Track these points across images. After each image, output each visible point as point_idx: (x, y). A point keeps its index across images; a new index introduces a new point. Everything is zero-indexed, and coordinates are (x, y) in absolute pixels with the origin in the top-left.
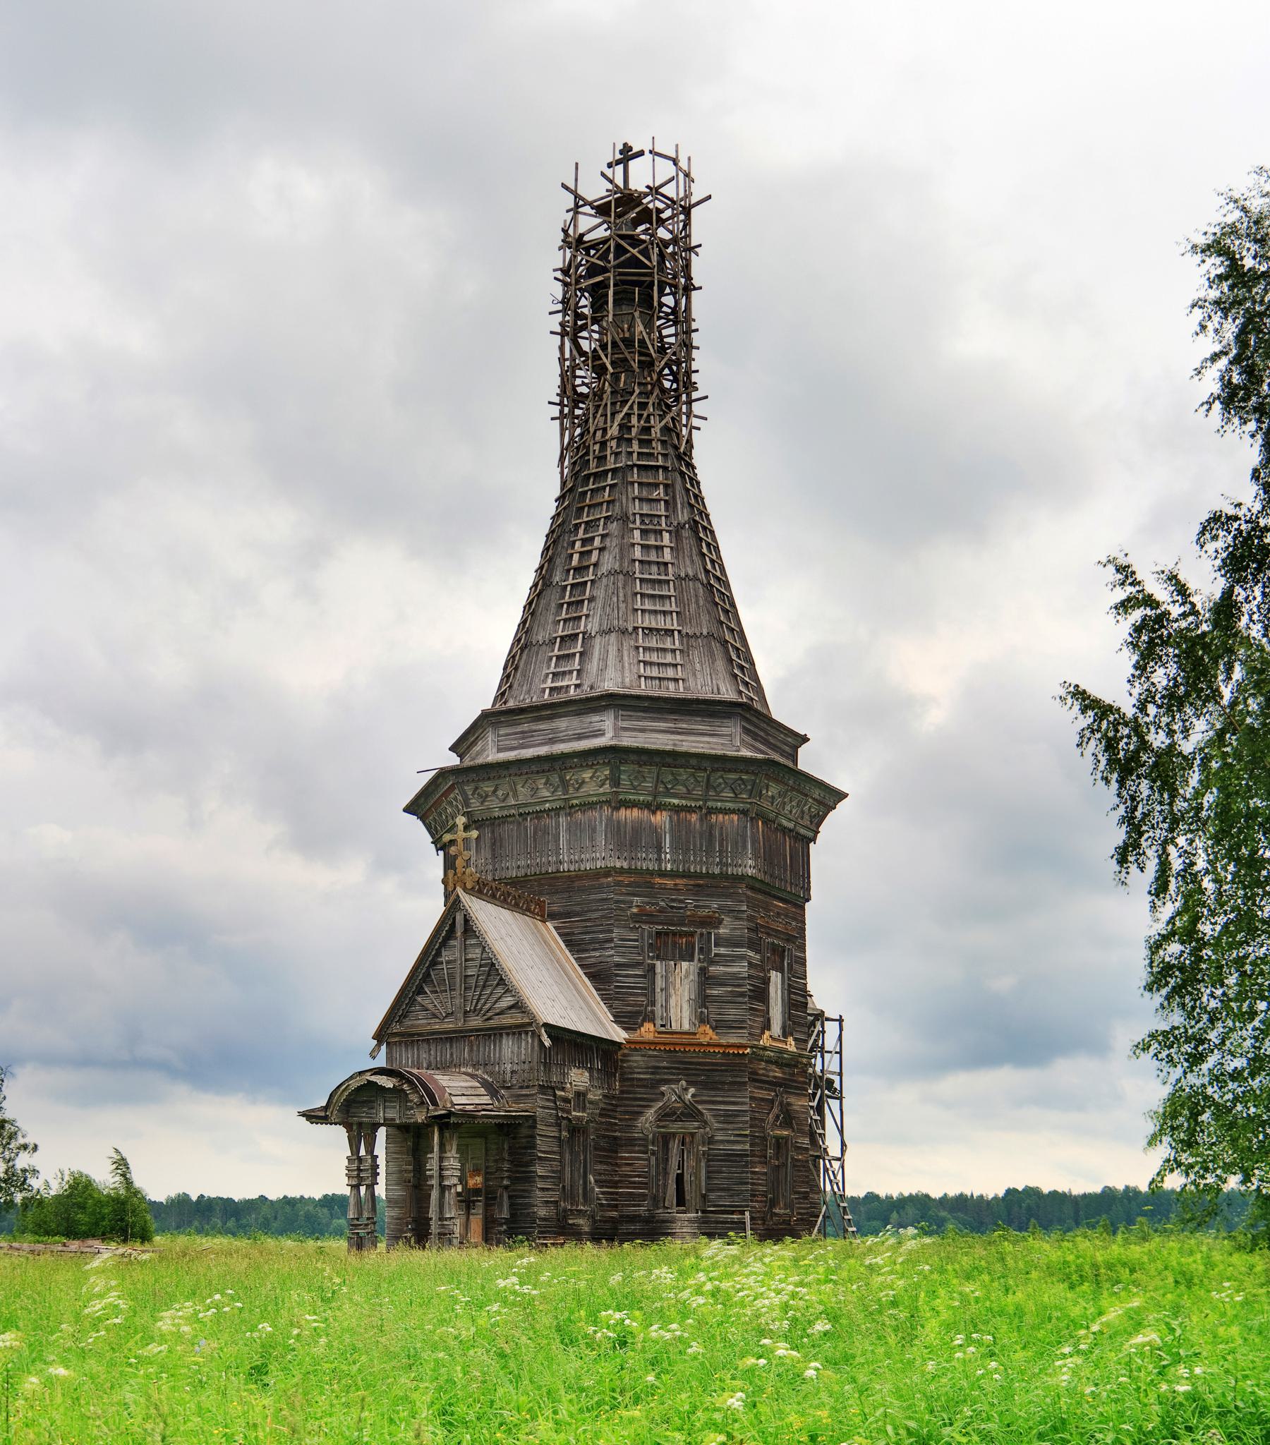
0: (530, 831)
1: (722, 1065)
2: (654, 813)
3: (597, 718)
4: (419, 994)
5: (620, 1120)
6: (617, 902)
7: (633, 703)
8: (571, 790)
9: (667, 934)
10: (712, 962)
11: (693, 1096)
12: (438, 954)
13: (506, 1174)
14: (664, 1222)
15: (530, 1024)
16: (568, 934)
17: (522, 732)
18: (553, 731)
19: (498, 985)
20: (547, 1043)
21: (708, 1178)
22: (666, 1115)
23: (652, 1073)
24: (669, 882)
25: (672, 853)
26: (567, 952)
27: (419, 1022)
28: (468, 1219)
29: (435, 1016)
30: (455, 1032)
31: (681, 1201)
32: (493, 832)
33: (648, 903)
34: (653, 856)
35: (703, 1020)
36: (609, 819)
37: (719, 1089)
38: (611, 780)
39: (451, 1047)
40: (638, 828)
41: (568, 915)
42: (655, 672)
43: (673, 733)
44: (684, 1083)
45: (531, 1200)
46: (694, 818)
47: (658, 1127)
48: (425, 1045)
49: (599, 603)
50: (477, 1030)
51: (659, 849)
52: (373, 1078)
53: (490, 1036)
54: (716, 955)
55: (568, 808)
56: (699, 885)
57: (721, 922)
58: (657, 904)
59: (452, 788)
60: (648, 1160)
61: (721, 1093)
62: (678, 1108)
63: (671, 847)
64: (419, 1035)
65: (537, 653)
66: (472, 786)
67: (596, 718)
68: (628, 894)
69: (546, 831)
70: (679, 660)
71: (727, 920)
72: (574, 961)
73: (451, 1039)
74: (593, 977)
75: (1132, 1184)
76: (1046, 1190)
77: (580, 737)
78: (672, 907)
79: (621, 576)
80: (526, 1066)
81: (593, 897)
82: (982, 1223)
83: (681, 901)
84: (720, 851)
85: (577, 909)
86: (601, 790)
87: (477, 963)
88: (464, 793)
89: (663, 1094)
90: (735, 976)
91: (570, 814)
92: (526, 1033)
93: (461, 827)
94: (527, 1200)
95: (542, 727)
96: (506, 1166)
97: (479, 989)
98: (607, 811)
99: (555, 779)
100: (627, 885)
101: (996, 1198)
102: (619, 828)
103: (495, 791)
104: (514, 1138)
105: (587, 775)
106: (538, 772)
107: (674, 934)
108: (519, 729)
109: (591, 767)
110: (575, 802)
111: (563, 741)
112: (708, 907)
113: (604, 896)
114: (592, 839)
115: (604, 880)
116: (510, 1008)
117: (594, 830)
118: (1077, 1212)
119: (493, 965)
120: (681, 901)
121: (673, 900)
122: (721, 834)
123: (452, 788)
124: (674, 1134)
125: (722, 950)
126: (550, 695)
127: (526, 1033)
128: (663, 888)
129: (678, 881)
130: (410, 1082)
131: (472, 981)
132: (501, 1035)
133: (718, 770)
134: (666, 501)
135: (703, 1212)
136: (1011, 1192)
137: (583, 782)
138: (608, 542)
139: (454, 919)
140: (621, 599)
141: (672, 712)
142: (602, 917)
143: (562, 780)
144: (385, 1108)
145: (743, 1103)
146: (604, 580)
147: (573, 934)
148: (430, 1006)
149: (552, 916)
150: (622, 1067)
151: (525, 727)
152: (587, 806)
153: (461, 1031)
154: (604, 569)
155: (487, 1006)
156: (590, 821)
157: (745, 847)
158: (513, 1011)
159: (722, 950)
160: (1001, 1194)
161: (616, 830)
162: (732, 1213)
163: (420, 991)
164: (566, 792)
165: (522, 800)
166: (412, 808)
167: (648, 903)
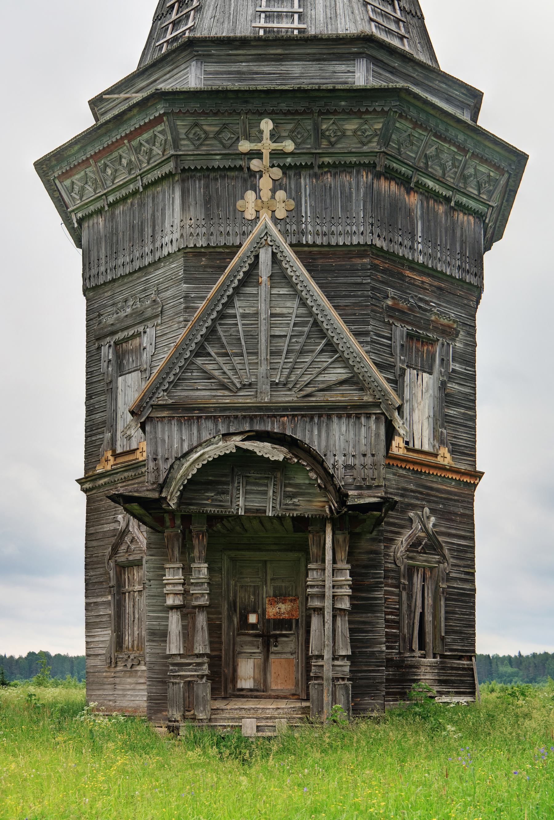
1: (455, 494)
3: (343, 68)
4: (198, 354)
6: (373, 289)
8: (325, 143)
10: (451, 379)
11: (434, 525)
12: (230, 304)
15: (377, 405)
17: (239, 72)
19: (322, 351)
21: (446, 619)
23: (402, 496)
27: (201, 393)
28: (266, 659)
29: (224, 387)
30: (259, 409)
31: (422, 646)
32: (207, 187)
35: (441, 440)
44: (426, 510)
45: (370, 636)
46: (441, 209)
47: (409, 558)
50: (294, 409)
52: (248, 445)
53: (312, 418)
54: (454, 371)
58: (406, 300)
59: (158, 120)
60: (399, 595)
64: (201, 410)
66: (190, 120)
70: (403, 31)
75: (44, 650)
76: (53, 654)
78: (420, 307)
80: (369, 460)
81: (342, 280)
82: (12, 673)
86: (365, 149)
88: (174, 130)
89: (411, 520)
91: (316, 176)
93: (266, 135)
94: (370, 636)
95: (266, 69)
98: (365, 178)
99: (308, 124)
100: (384, 271)
101: (20, 658)
103: (219, 133)
105: (351, 126)
106: (289, 113)
108: (234, 68)
109: (359, 114)
110: (327, 160)
113: (359, 280)
116: (342, 383)
118: (72, 667)
119: (316, 323)
121: (421, 300)
123: (158, 120)
124: (418, 567)
129: (425, 279)
131: (284, 345)
132: (329, 417)
135: (443, 656)
136: (31, 655)
139: (257, 257)
143: (316, 128)
144: (247, 493)
148: (216, 373)
151: (243, 67)
152: (339, 168)
153: (268, 409)
155: (307, 378)
160: (24, 655)
162: (460, 658)
163: (201, 352)
164: (318, 144)
166: (45, 167)
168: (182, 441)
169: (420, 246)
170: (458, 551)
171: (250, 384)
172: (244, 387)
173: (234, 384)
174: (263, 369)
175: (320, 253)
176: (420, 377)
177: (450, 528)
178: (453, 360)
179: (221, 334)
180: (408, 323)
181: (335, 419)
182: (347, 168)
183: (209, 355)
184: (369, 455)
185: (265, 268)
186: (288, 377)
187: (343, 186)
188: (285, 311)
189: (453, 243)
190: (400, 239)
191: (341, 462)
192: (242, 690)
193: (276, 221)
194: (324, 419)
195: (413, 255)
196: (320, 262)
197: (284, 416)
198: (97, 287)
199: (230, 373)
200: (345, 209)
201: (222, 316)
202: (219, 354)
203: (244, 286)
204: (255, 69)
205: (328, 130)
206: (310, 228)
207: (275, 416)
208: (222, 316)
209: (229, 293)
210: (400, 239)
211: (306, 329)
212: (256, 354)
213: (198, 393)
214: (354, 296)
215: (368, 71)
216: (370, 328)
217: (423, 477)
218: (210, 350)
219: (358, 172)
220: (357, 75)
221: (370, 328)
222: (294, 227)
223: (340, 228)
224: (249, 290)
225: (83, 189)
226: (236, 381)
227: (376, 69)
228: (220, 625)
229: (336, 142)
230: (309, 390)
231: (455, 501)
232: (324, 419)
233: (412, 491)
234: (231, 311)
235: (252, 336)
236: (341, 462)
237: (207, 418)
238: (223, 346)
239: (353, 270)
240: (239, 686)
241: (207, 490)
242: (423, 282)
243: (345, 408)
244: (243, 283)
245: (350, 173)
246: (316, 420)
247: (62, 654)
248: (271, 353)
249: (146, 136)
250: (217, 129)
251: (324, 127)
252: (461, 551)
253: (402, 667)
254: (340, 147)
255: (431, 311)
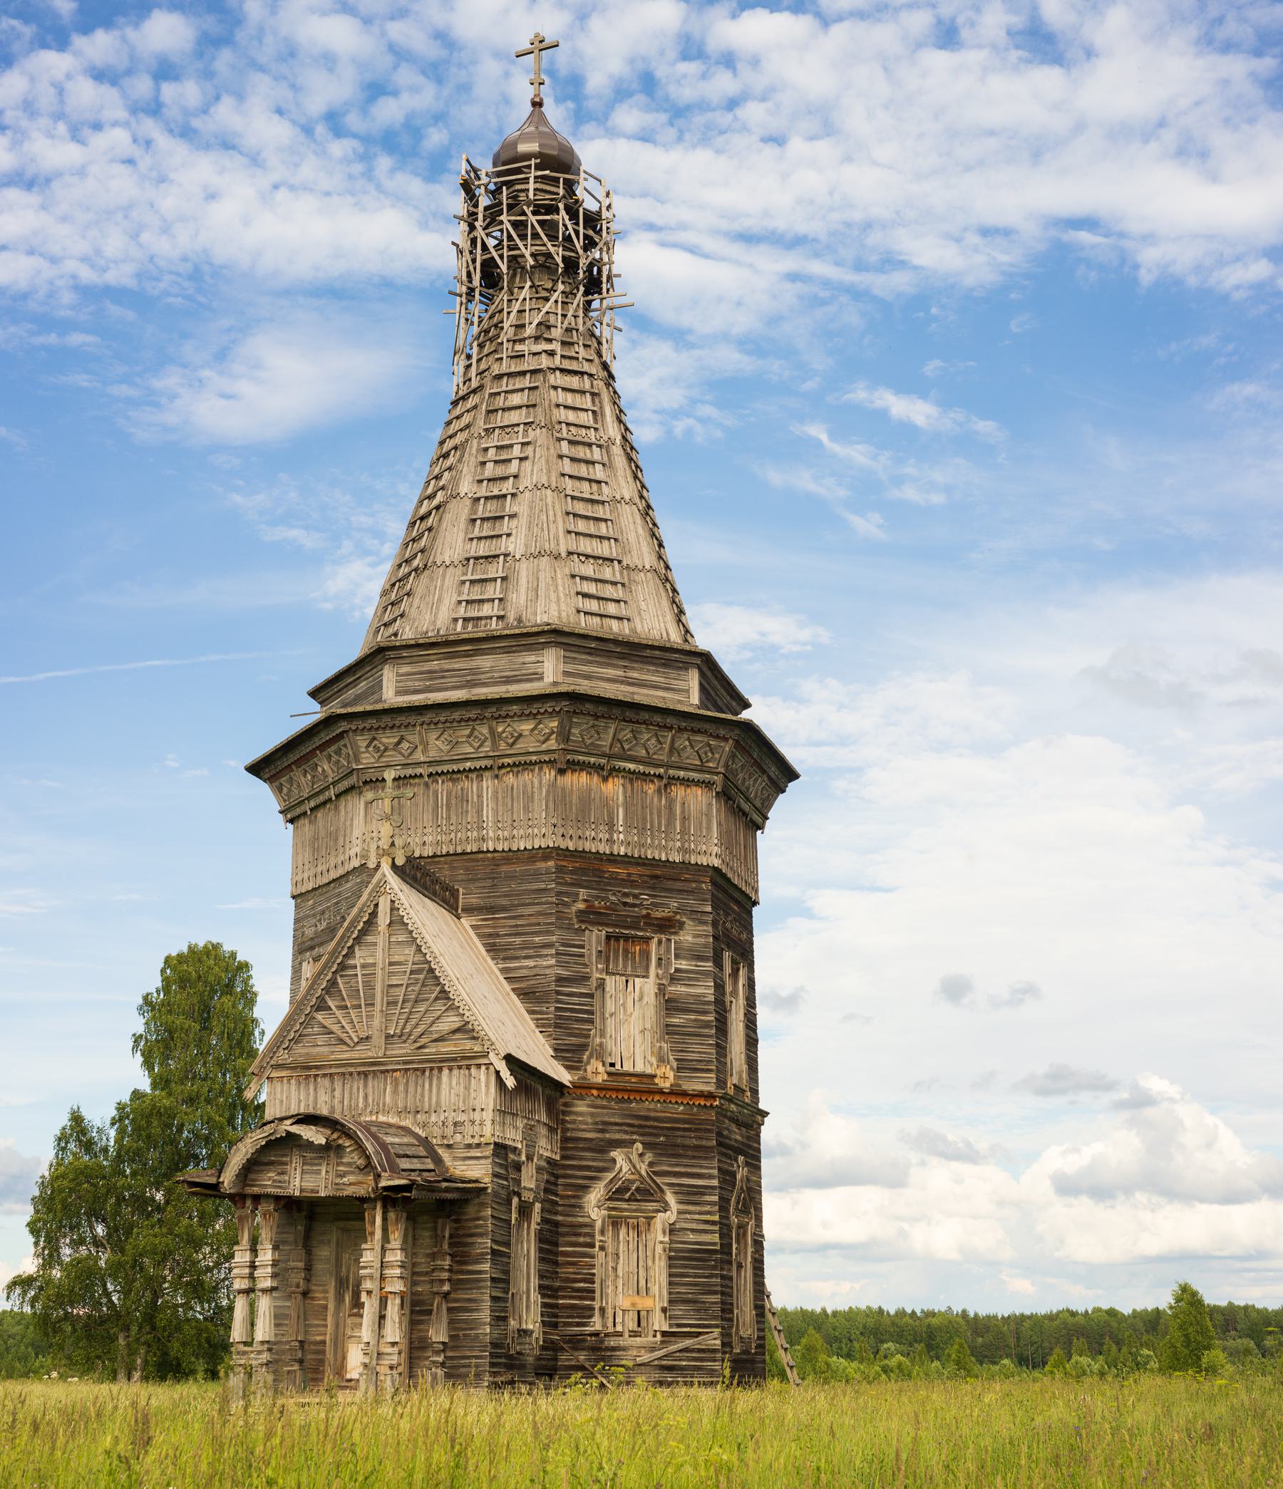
0: (443, 799)
2: (605, 779)
3: (533, 658)
4: (319, 1009)
5: (562, 1197)
7: (578, 642)
8: (503, 745)
9: (617, 939)
10: (673, 979)
13: (445, 1275)
14: (614, 1349)
16: (490, 935)
18: (473, 671)
19: (437, 999)
20: (510, 1082)
22: (618, 1194)
24: (621, 871)
25: (627, 832)
26: (489, 959)
27: (319, 1049)
29: (342, 1042)
33: (597, 897)
34: (604, 836)
36: (553, 785)
37: (680, 1156)
38: (560, 734)
39: (366, 1086)
40: (586, 800)
41: (491, 909)
42: (593, 606)
43: (622, 682)
44: (639, 1146)
45: (475, 1315)
48: (327, 1082)
49: (523, 520)
51: (611, 826)
52: (295, 1129)
53: (424, 1071)
54: (677, 970)
55: (496, 768)
56: (656, 877)
57: (681, 925)
61: (686, 1161)
62: (633, 1182)
63: (625, 824)
64: (317, 1067)
65: (444, 576)
66: (367, 737)
67: (530, 658)
68: (572, 885)
69: (464, 799)
71: (689, 924)
72: (498, 973)
73: (366, 1074)
74: (526, 995)
77: (508, 681)
78: (625, 904)
79: (549, 491)
83: (636, 896)
84: (682, 832)
85: (504, 902)
86: (544, 747)
87: (409, 968)
90: (698, 999)
92: (479, 1066)
95: (456, 666)
96: (447, 1263)
97: (409, 1005)
98: (549, 775)
102: (564, 797)
103: (399, 743)
104: (457, 1221)
105: (526, 727)
107: (626, 938)
110: (507, 761)
111: (485, 685)
112: (667, 906)
113: (543, 886)
114: (527, 809)
115: (541, 865)
117: (531, 798)
119: (431, 971)
120: (636, 896)
121: (626, 895)
122: (683, 812)
125: (683, 964)
126: (464, 627)
127: (479, 1066)
128: (615, 880)
130: (348, 1134)
132: (440, 1069)
133: (685, 729)
134: (594, 412)
137: (520, 735)
138: (529, 451)
140: (551, 518)
141: (622, 656)
142: (539, 914)
143: (492, 731)
145: (711, 1177)
146: (527, 494)
147: (498, 935)
148: (335, 1028)
149: (469, 910)
150: (564, 1121)
151: (435, 665)
152: (521, 767)
154: (525, 482)
155: (420, 1029)
156: (525, 786)
157: (709, 829)
158: (458, 1036)
159: (683, 964)
161: (559, 800)
163: (321, 1006)
164: (495, 746)
165: (433, 754)
167: (597, 897)
168: (300, 1101)
169: (621, 836)
170: (689, 1194)
171: (367, 1038)
172: (361, 1040)
173: (351, 1038)
174: (377, 1022)
175: (504, 859)
176: (630, 983)
177: (677, 1165)
178: (677, 957)
179: (341, 986)
180: (607, 925)
181: (446, 1071)
182: (528, 766)
183: (330, 1009)
184: (478, 1110)
185: (383, 919)
186: (403, 1028)
187: (525, 786)
188: (402, 958)
189: (670, 822)
190: (593, 834)
191: (450, 1119)
192: (350, 1380)
193: (394, 867)
194: (435, 1072)
195: (611, 847)
196: (504, 868)
197: (396, 1070)
198: (301, 895)
199: (348, 1027)
200: (527, 809)
201: (343, 967)
202: (340, 1008)
203: (365, 935)
204: (447, 667)
205: (504, 731)
206: (491, 834)
207: (387, 1071)
208: (343, 967)
209: (349, 944)
210: (593, 834)
211: (422, 976)
212: (373, 1005)
213: (318, 1049)
214: (538, 904)
215: (557, 659)
216: (554, 938)
217: (633, 1105)
218: (331, 1003)
219: (540, 769)
220: (546, 664)
221: (554, 938)
222: (475, 834)
223: (522, 832)
224: (369, 939)
225: (290, 790)
226: (353, 1035)
227: (568, 654)
228: (326, 1307)
229: (513, 743)
230: (423, 1041)
231: (685, 1130)
232: (435, 1072)
233: (616, 1124)
234: (351, 962)
235: (369, 986)
236: (450, 1119)
237: (324, 1075)
238: (343, 999)
239: (537, 875)
240: (348, 1376)
241: (269, 1171)
242: (629, 875)
243: (454, 1060)
244: (364, 932)
245: (532, 771)
246: (427, 1073)
247: (1126, 1310)
248: (388, 1003)
249: (333, 748)
250: (396, 740)
251: (500, 729)
252: (696, 1194)
253: (600, 1349)
254: (520, 746)
255: (641, 904)
